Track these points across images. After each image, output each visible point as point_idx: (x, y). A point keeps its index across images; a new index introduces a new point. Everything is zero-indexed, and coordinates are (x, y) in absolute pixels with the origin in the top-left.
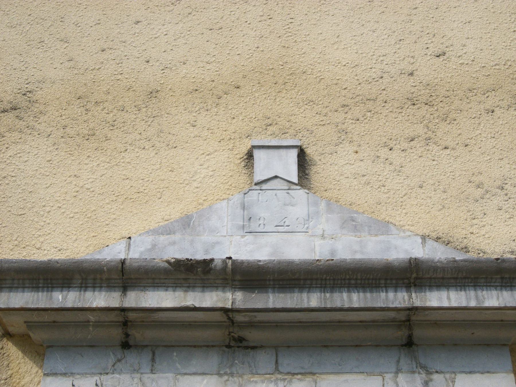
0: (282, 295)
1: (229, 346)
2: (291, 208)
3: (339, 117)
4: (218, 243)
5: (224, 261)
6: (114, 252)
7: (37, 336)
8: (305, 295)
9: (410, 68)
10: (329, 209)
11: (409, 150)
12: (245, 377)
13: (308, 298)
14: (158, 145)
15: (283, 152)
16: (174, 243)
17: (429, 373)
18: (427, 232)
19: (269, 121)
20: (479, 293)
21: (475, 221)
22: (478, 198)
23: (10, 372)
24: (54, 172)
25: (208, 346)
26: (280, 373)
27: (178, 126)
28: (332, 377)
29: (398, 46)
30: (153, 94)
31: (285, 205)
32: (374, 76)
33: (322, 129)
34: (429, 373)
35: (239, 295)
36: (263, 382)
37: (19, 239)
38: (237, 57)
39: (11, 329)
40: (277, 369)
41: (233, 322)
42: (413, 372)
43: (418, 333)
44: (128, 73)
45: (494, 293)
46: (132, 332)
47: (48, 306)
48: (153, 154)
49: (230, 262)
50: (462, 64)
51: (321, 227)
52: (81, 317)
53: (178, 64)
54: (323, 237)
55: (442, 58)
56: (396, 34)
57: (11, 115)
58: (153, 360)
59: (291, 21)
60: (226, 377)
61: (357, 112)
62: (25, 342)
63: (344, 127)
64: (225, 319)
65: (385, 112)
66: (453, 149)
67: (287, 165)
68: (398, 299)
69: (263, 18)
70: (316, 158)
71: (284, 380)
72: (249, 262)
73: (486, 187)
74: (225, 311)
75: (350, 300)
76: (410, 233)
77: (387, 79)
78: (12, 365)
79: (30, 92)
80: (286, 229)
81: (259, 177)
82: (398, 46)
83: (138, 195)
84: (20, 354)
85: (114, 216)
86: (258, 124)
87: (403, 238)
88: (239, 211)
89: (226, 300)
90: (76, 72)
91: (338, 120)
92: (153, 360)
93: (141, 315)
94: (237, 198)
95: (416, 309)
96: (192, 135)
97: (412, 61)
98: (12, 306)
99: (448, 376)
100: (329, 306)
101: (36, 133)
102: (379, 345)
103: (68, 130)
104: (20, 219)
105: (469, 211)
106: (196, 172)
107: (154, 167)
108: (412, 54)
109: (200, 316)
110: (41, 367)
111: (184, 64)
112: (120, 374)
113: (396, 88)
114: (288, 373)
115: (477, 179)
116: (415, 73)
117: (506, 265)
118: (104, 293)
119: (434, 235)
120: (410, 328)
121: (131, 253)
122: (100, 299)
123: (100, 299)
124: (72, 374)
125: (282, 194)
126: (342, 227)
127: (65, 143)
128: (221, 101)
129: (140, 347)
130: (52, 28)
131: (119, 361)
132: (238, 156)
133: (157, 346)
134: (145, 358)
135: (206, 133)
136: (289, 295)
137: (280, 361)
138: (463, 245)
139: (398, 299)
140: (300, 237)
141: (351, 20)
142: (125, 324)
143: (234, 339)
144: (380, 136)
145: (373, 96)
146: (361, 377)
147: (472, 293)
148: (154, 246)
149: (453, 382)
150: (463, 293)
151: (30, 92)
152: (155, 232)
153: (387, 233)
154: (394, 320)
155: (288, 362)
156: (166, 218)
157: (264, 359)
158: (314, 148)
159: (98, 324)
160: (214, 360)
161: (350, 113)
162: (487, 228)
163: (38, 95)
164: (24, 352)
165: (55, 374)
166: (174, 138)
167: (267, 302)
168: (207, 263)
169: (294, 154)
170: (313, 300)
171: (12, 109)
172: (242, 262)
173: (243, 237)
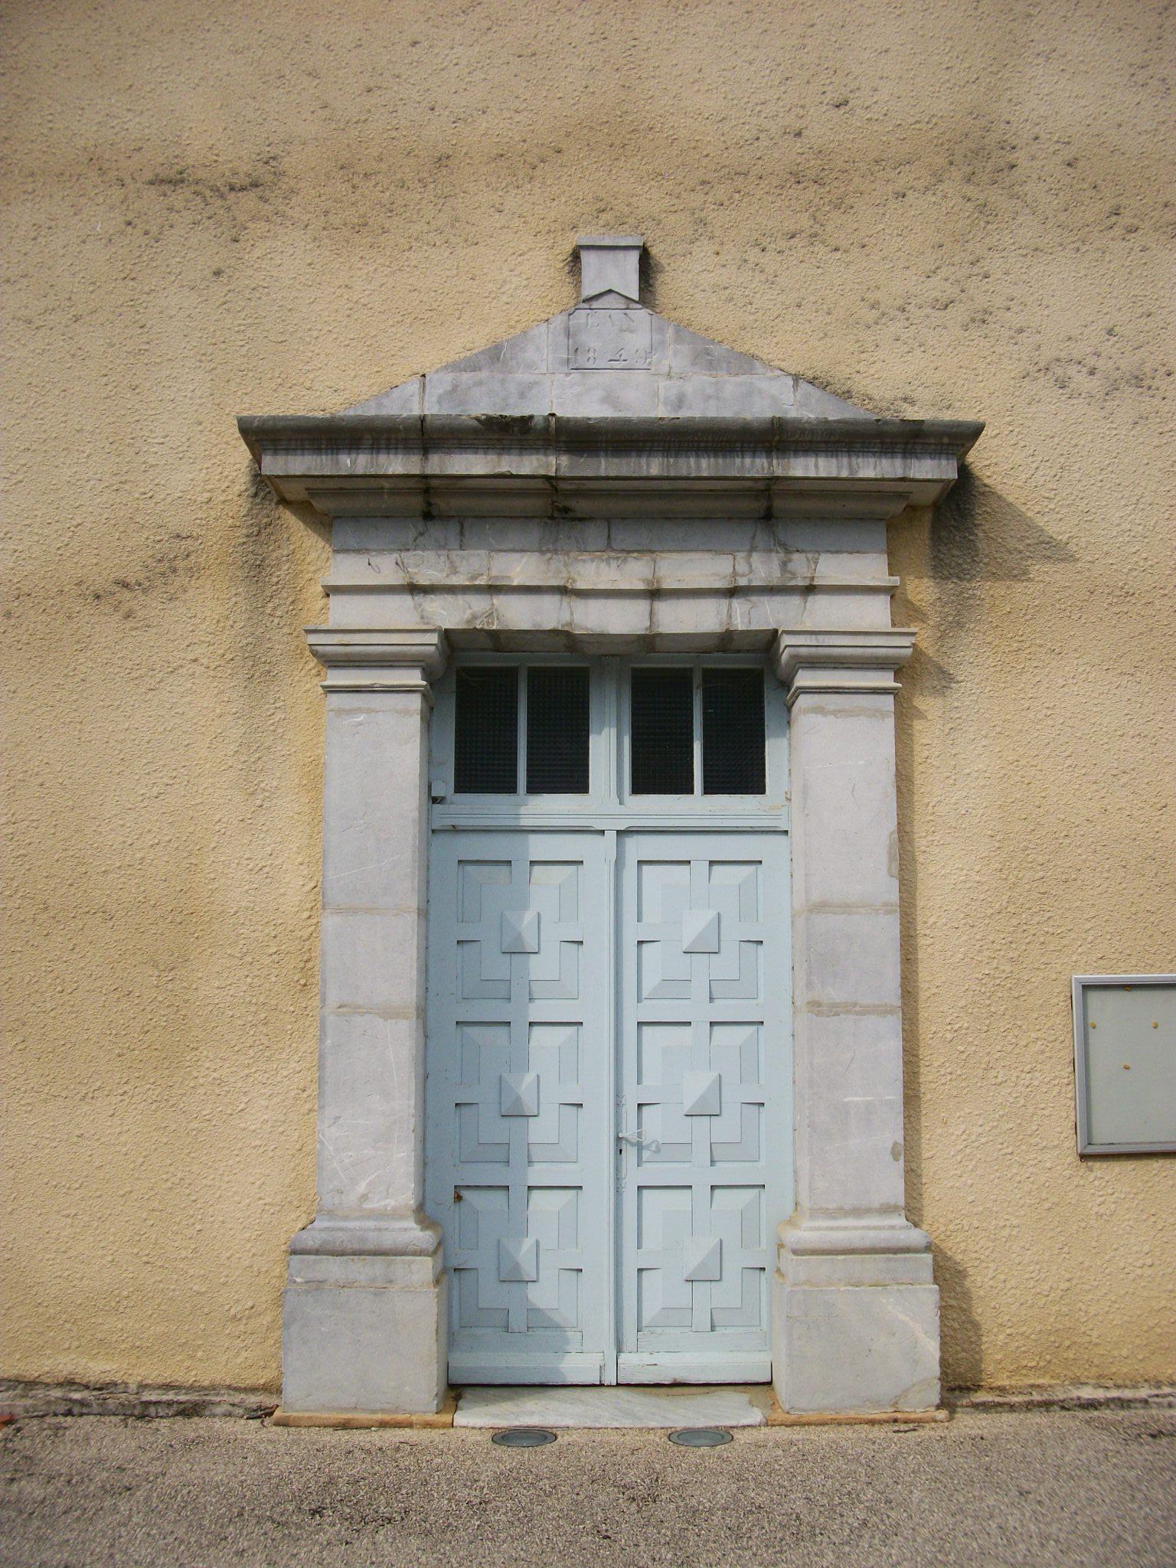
0: (616, 460)
1: (552, 518)
2: (630, 335)
3: (696, 199)
4: (536, 383)
5: (546, 419)
6: (409, 404)
7: (319, 505)
8: (644, 460)
9: (798, 125)
10: (679, 337)
11: (787, 252)
12: (572, 555)
13: (648, 465)
14: (453, 240)
15: (620, 254)
16: (480, 383)
17: (788, 552)
18: (800, 369)
19: (601, 205)
20: (854, 460)
21: (863, 356)
22: (871, 322)
23: (292, 547)
24: (318, 280)
25: (527, 517)
26: (613, 550)
27: (478, 211)
28: (675, 555)
29: (783, 89)
30: (442, 161)
31: (621, 330)
32: (748, 136)
33: (673, 218)
34: (788, 552)
35: (564, 460)
36: (593, 561)
37: (283, 376)
38: (558, 102)
39: (288, 496)
40: (609, 547)
41: (556, 490)
42: (771, 551)
43: (778, 504)
44: (406, 128)
45: (872, 460)
46: (435, 500)
47: (335, 473)
48: (447, 254)
49: (553, 420)
50: (869, 120)
51: (666, 362)
52: (373, 483)
53: (475, 113)
54: (669, 376)
55: (842, 110)
56: (781, 68)
57: (252, 194)
58: (462, 534)
59: (634, 43)
60: (549, 555)
61: (721, 192)
62: (304, 509)
63: (703, 215)
64: (548, 486)
65: (759, 193)
66: (846, 251)
67: (624, 274)
68: (755, 466)
69: (594, 38)
70: (664, 262)
71: (618, 558)
72: (576, 420)
73: (882, 307)
74: (548, 478)
75: (699, 467)
76: (779, 373)
77: (764, 142)
78: (293, 539)
79: (274, 158)
80: (622, 364)
81: (588, 291)
82: (783, 89)
83: (431, 314)
84: (302, 526)
85: (401, 344)
86: (586, 210)
87: (771, 379)
88: (562, 339)
89: (548, 465)
90: (334, 126)
91: (694, 205)
92: (462, 534)
93: (447, 481)
94: (559, 321)
95: (778, 478)
96: (498, 225)
97: (801, 112)
98: (292, 473)
99: (810, 556)
100: (672, 474)
101: (289, 223)
102: (731, 518)
103: (331, 217)
104: (280, 348)
105: (858, 341)
106: (505, 281)
107: (448, 273)
108: (802, 102)
109: (518, 483)
110: (328, 541)
111: (484, 113)
112: (423, 550)
113: (776, 155)
114: (623, 551)
115: (871, 297)
116: (805, 133)
117: (886, 428)
118: (400, 456)
119: (810, 374)
120: (770, 498)
121: (426, 404)
122: (396, 464)
123: (396, 464)
124: (367, 550)
125: (617, 315)
126: (694, 364)
127: (329, 237)
128: (537, 172)
129: (445, 518)
130: (294, 54)
131: (422, 534)
132: (561, 258)
133: (466, 517)
134: (453, 529)
135: (517, 222)
136: (624, 461)
137: (613, 536)
138: (845, 388)
139: (755, 466)
140: (640, 376)
141: (719, 43)
142: (427, 491)
143: (559, 510)
144: (751, 230)
145: (744, 169)
146: (707, 556)
147: (845, 461)
148: (455, 388)
149: (816, 563)
150: (834, 460)
151: (274, 158)
152: (455, 367)
153: (750, 371)
154: (750, 490)
155: (623, 536)
156: (469, 346)
157: (594, 533)
158: (662, 247)
159: (395, 492)
160: (534, 533)
161: (711, 194)
162: (878, 365)
163: (286, 164)
164: (305, 522)
165: (347, 551)
166: (474, 229)
167: (598, 468)
168: (525, 421)
169: (634, 257)
170: (654, 466)
171: (252, 185)
172: (568, 420)
173: (568, 374)
